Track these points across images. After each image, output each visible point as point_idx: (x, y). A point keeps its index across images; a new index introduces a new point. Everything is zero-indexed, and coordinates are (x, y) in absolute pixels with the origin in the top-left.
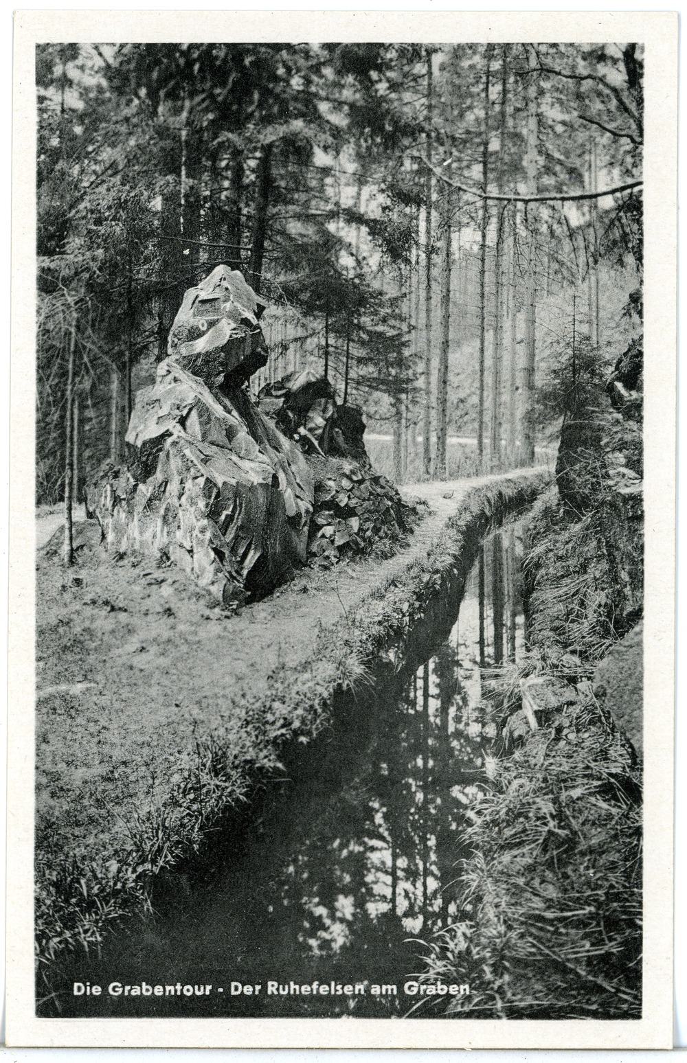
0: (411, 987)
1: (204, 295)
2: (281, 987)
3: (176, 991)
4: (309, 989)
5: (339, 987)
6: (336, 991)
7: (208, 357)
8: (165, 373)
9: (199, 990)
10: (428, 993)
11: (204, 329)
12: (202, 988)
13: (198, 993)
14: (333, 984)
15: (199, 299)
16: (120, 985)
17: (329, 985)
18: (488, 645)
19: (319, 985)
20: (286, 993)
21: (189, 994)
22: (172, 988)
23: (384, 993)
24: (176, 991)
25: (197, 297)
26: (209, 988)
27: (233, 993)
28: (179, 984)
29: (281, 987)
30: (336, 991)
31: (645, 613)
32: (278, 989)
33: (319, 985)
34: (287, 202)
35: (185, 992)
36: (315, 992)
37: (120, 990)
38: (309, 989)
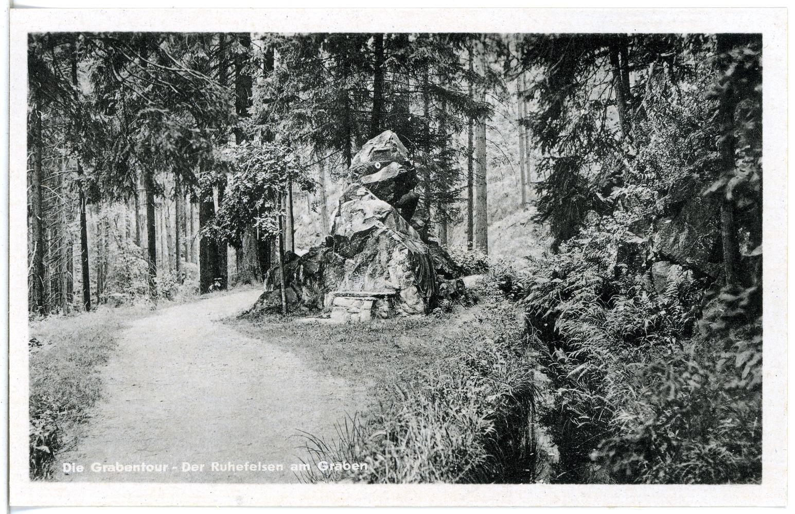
0: (96, 466)
1: (379, 147)
2: (221, 466)
3: (141, 468)
4: (242, 467)
5: (264, 466)
6: (262, 468)
7: (384, 184)
8: (363, 194)
9: (224, 468)
10: (109, 470)
11: (379, 167)
12: (160, 466)
13: (157, 470)
14: (260, 463)
15: (375, 150)
16: (99, 464)
17: (257, 464)
18: (143, 191)
19: (250, 464)
20: (225, 469)
21: (150, 471)
22: (138, 466)
23: (278, 469)
24: (141, 468)
25: (373, 148)
26: (165, 466)
27: (184, 470)
28: (143, 463)
29: (221, 466)
30: (262, 468)
31: (763, 362)
32: (219, 467)
33: (250, 464)
34: (606, 209)
35: (238, 469)
36: (246, 469)
37: (100, 469)
38: (242, 467)
